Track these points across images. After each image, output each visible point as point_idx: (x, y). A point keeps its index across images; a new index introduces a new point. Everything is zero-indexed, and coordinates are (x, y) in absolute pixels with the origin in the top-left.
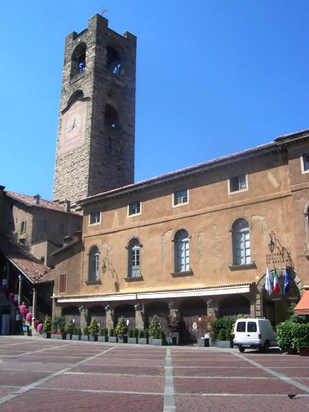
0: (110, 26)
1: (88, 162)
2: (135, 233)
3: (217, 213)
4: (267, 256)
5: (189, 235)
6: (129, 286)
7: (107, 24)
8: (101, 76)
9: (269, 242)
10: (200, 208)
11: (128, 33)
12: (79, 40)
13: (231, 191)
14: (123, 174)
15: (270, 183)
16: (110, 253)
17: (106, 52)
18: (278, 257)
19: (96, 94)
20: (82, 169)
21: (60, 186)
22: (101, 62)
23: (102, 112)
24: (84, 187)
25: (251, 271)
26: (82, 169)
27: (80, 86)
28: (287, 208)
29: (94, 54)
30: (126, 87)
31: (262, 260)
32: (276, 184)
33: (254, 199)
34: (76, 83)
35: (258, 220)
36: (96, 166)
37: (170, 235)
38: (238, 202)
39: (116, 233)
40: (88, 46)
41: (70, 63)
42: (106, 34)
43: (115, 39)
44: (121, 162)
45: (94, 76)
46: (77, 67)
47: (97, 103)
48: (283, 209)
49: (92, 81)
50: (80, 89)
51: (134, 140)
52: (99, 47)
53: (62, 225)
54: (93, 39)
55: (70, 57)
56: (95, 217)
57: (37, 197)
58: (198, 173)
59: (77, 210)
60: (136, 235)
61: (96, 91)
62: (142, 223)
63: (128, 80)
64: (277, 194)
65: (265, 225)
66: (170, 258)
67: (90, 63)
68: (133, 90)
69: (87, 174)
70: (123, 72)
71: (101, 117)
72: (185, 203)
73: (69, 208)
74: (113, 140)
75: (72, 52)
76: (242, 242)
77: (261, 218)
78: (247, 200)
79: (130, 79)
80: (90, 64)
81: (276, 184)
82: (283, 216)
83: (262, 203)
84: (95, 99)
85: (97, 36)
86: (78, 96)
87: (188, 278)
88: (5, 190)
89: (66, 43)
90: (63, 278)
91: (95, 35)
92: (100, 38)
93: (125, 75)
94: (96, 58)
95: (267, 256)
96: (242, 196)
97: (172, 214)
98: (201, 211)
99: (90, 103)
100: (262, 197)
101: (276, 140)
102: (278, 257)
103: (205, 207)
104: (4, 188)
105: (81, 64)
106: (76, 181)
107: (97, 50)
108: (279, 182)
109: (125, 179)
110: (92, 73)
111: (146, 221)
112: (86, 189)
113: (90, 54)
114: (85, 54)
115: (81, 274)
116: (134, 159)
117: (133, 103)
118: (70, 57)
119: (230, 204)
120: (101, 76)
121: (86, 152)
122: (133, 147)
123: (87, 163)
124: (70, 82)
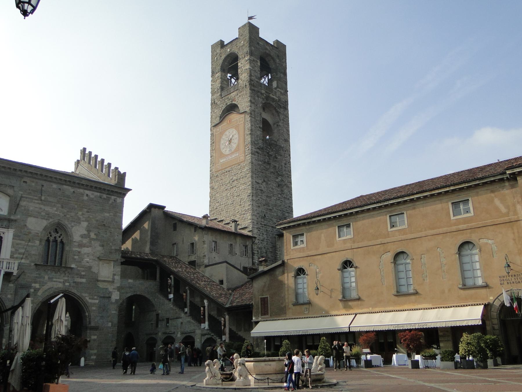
0: (261, 35)
1: (250, 179)
2: (348, 256)
3: (441, 237)
4: (500, 277)
5: (306, 273)
7: (258, 33)
8: (256, 89)
9: (504, 264)
10: (421, 231)
11: (277, 42)
12: (228, 50)
13: (454, 216)
14: (282, 191)
15: (497, 209)
16: (319, 276)
17: (259, 64)
18: (513, 278)
19: (253, 108)
20: (243, 187)
22: (256, 74)
24: (247, 205)
25: (483, 291)
26: (243, 187)
27: (234, 100)
28: (518, 232)
29: (248, 66)
30: (279, 100)
31: (494, 282)
32: (504, 210)
33: (480, 224)
34: (229, 96)
35: (487, 243)
36: (258, 183)
37: (389, 257)
38: (461, 227)
39: (325, 255)
40: (240, 57)
42: (258, 44)
43: (266, 49)
44: (280, 178)
45: (250, 89)
47: (255, 118)
48: (514, 233)
49: (248, 95)
51: (290, 155)
52: (252, 58)
53: (231, 245)
54: (246, 49)
55: (219, 68)
58: (416, 198)
61: (253, 105)
62: (356, 245)
63: (281, 93)
64: (506, 219)
65: (495, 248)
66: (390, 280)
67: (243, 75)
68: (286, 102)
69: (250, 191)
70: (275, 84)
74: (271, 155)
75: (221, 61)
78: (473, 224)
79: (282, 91)
81: (504, 210)
82: (514, 240)
83: (489, 227)
84: (252, 114)
85: (250, 46)
86: (232, 108)
87: (413, 298)
90: (264, 301)
91: (247, 45)
92: (253, 48)
93: (278, 87)
94: (250, 71)
95: (500, 277)
96: (466, 221)
97: (389, 237)
98: (423, 234)
99: (248, 118)
100: (489, 222)
102: (513, 278)
103: (425, 230)
104: (164, 207)
106: (238, 199)
107: (251, 62)
108: (507, 207)
109: (284, 196)
110: (248, 86)
112: (250, 206)
114: (237, 65)
115: (286, 297)
116: (291, 175)
117: (287, 117)
118: (219, 68)
119: (454, 228)
120: (256, 89)
121: (247, 169)
122: (290, 162)
123: (248, 180)
124: (221, 95)
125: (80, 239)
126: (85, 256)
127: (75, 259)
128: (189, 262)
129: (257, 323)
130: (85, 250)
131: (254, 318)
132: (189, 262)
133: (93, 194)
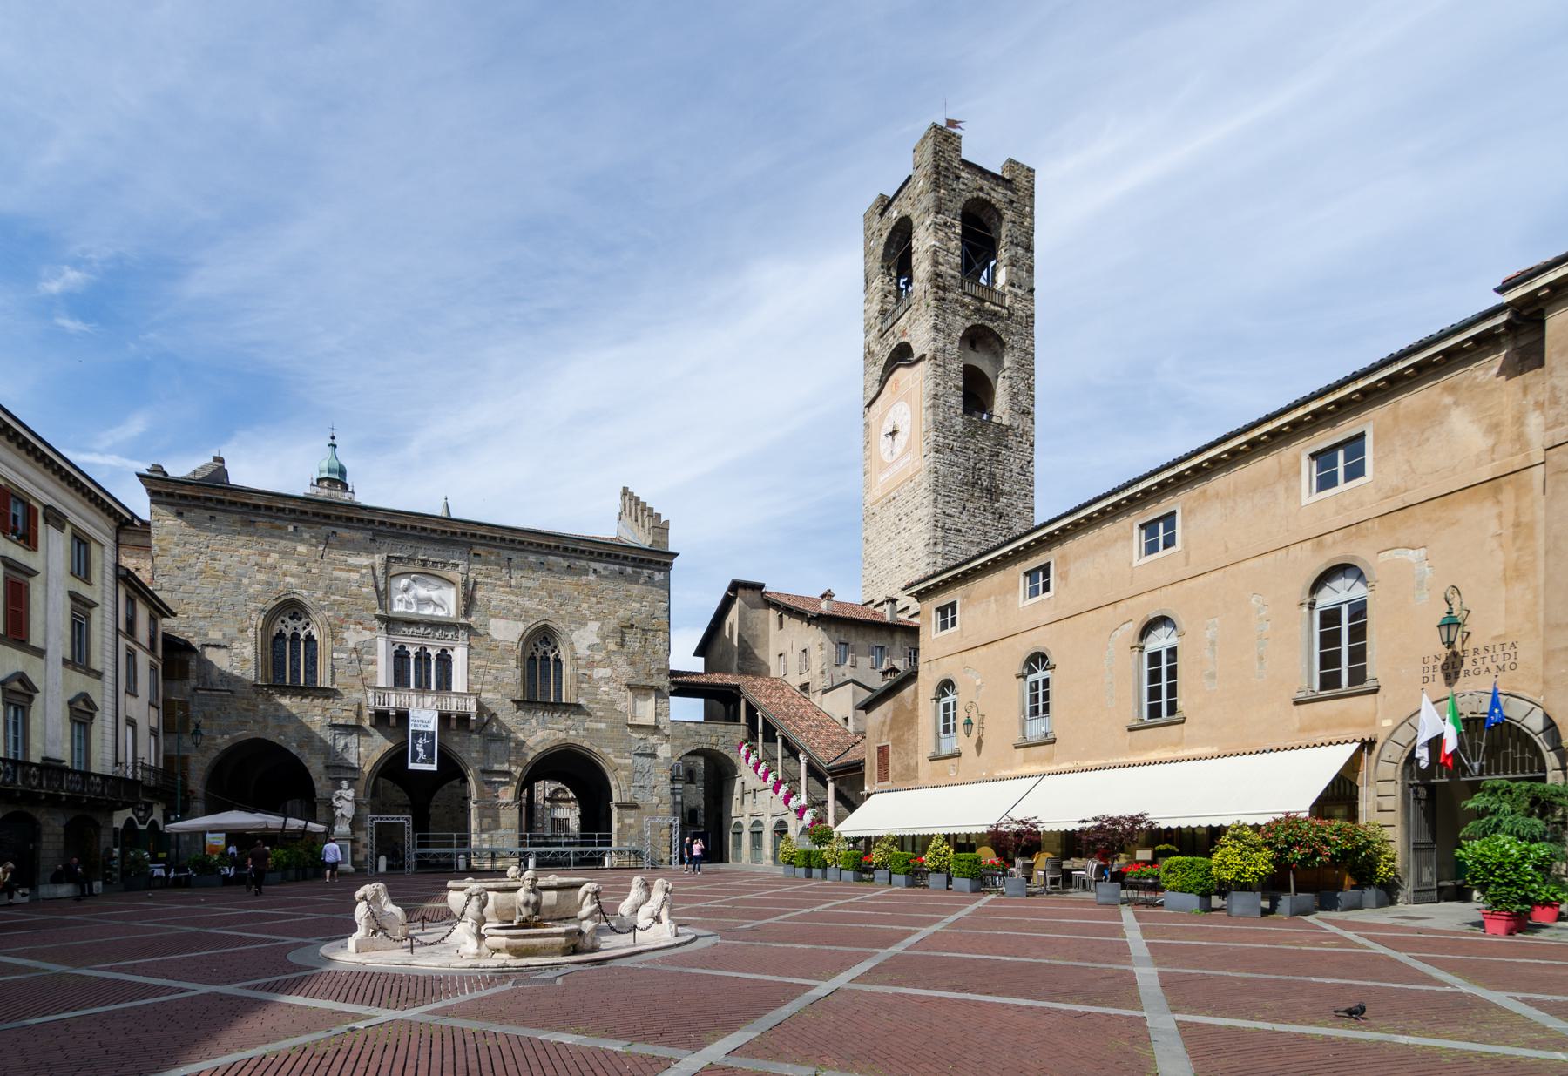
6: (1026, 761)
21: (876, 571)
23: (957, 387)
27: (904, 334)
41: (877, 283)
46: (894, 288)
50: (903, 340)
56: (1514, 532)
57: (827, 595)
59: (910, 617)
60: (1041, 646)
71: (956, 401)
72: (1047, 595)
73: (894, 612)
75: (880, 250)
76: (261, 629)
77: (1412, 555)
80: (922, 268)
86: (902, 355)
88: (1367, 739)
89: (867, 228)
101: (1501, 290)
105: (902, 281)
106: (908, 556)
111: (568, 668)
113: (923, 242)
114: (910, 247)
125: (589, 652)
126: (601, 683)
127: (583, 689)
128: (800, 687)
129: (869, 796)
130: (599, 673)
131: (866, 788)
132: (800, 687)
133: (605, 568)
